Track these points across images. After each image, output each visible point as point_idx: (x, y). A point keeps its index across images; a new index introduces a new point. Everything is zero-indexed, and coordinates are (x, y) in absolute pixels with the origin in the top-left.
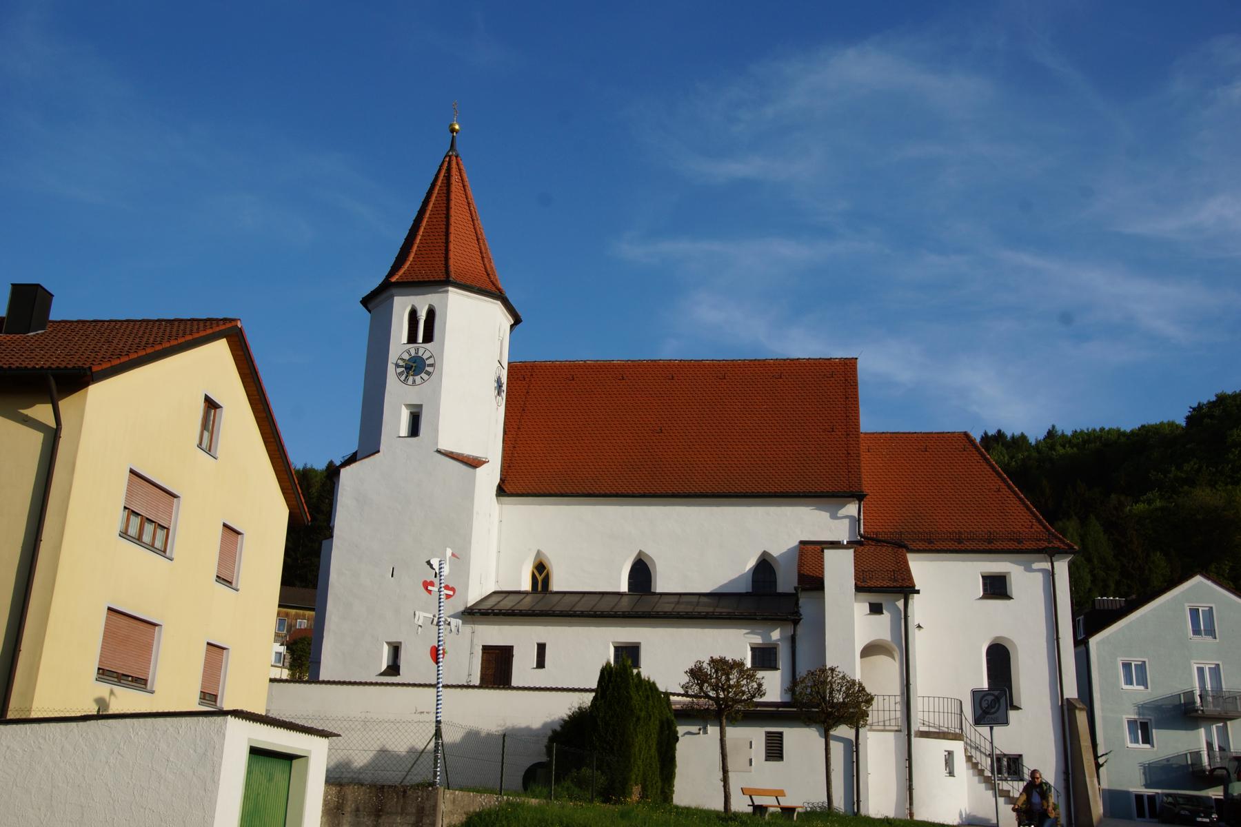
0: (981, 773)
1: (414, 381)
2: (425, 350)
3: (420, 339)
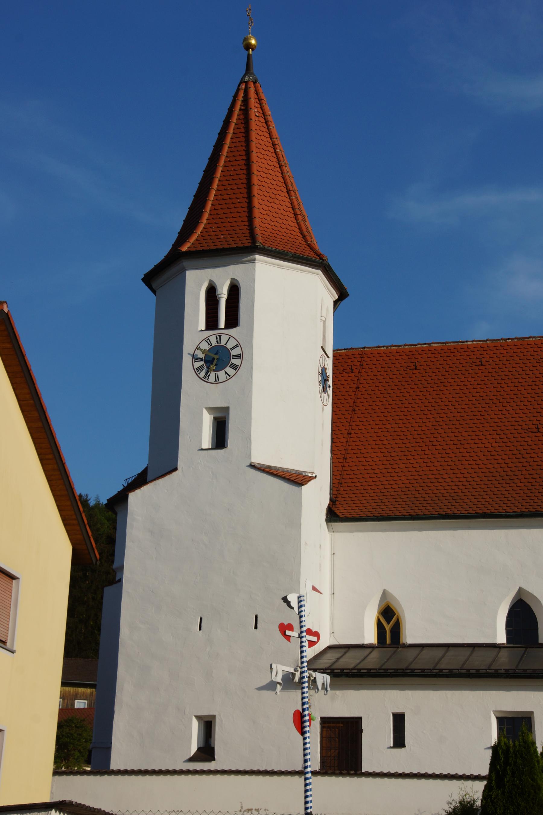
1: (217, 378)
2: (229, 338)
3: (222, 324)
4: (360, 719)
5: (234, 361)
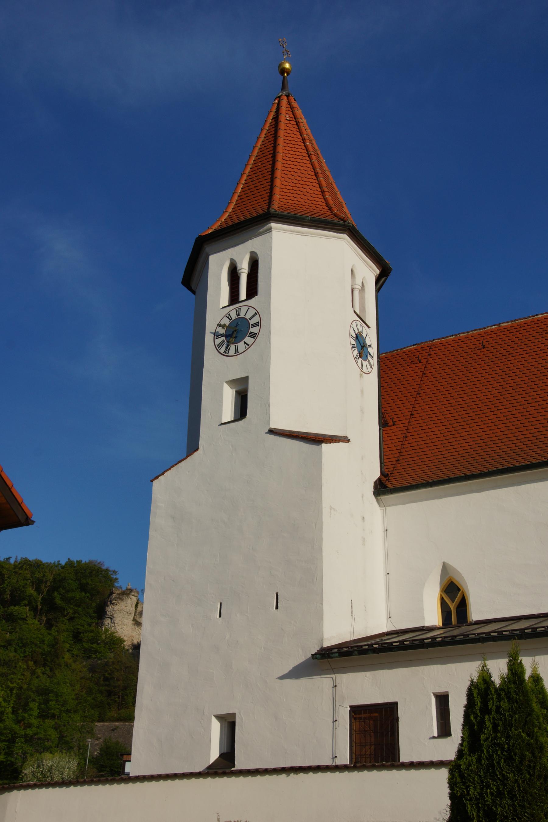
1: (237, 350)
3: (243, 295)
4: (396, 704)
5: (253, 330)
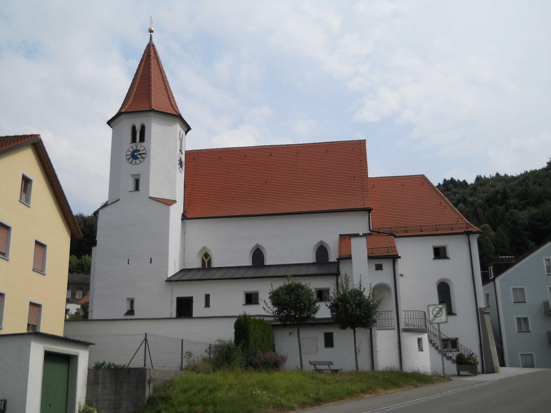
0: (437, 348)
1: (136, 162)
4: (361, 144)
